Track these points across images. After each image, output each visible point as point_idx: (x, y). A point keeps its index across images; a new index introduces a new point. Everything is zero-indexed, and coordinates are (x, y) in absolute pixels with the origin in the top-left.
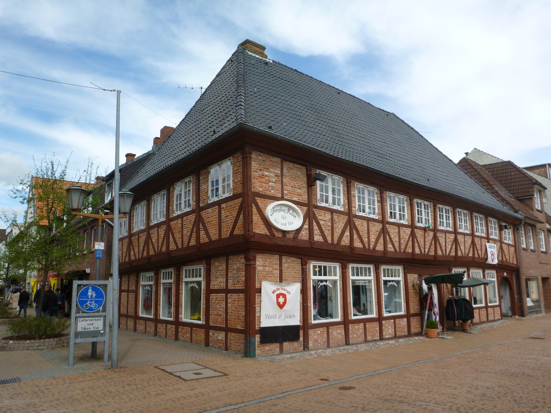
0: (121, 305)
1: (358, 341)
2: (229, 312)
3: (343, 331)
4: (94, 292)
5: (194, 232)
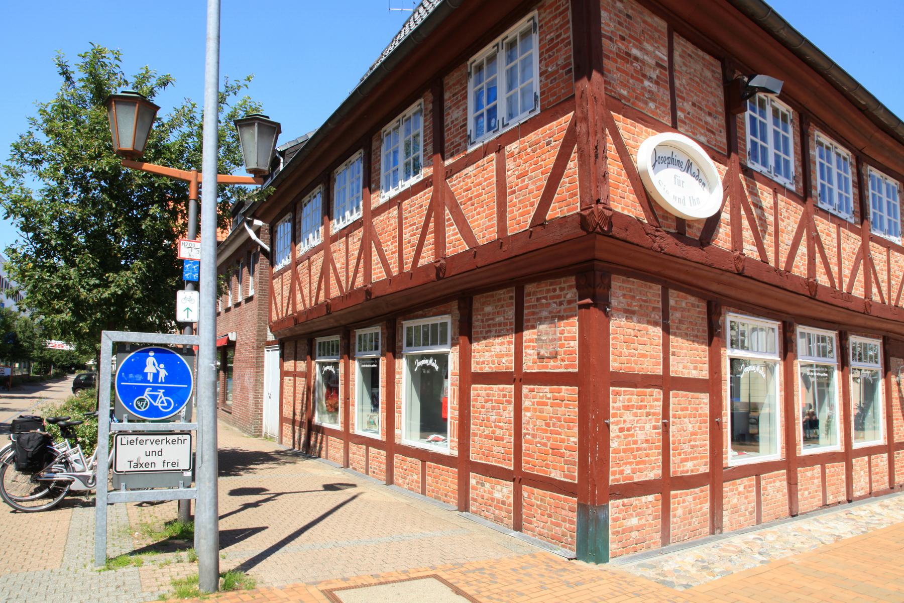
0: (284, 401)
1: (812, 507)
2: (526, 434)
3: (785, 483)
4: (162, 366)
5: (431, 233)
